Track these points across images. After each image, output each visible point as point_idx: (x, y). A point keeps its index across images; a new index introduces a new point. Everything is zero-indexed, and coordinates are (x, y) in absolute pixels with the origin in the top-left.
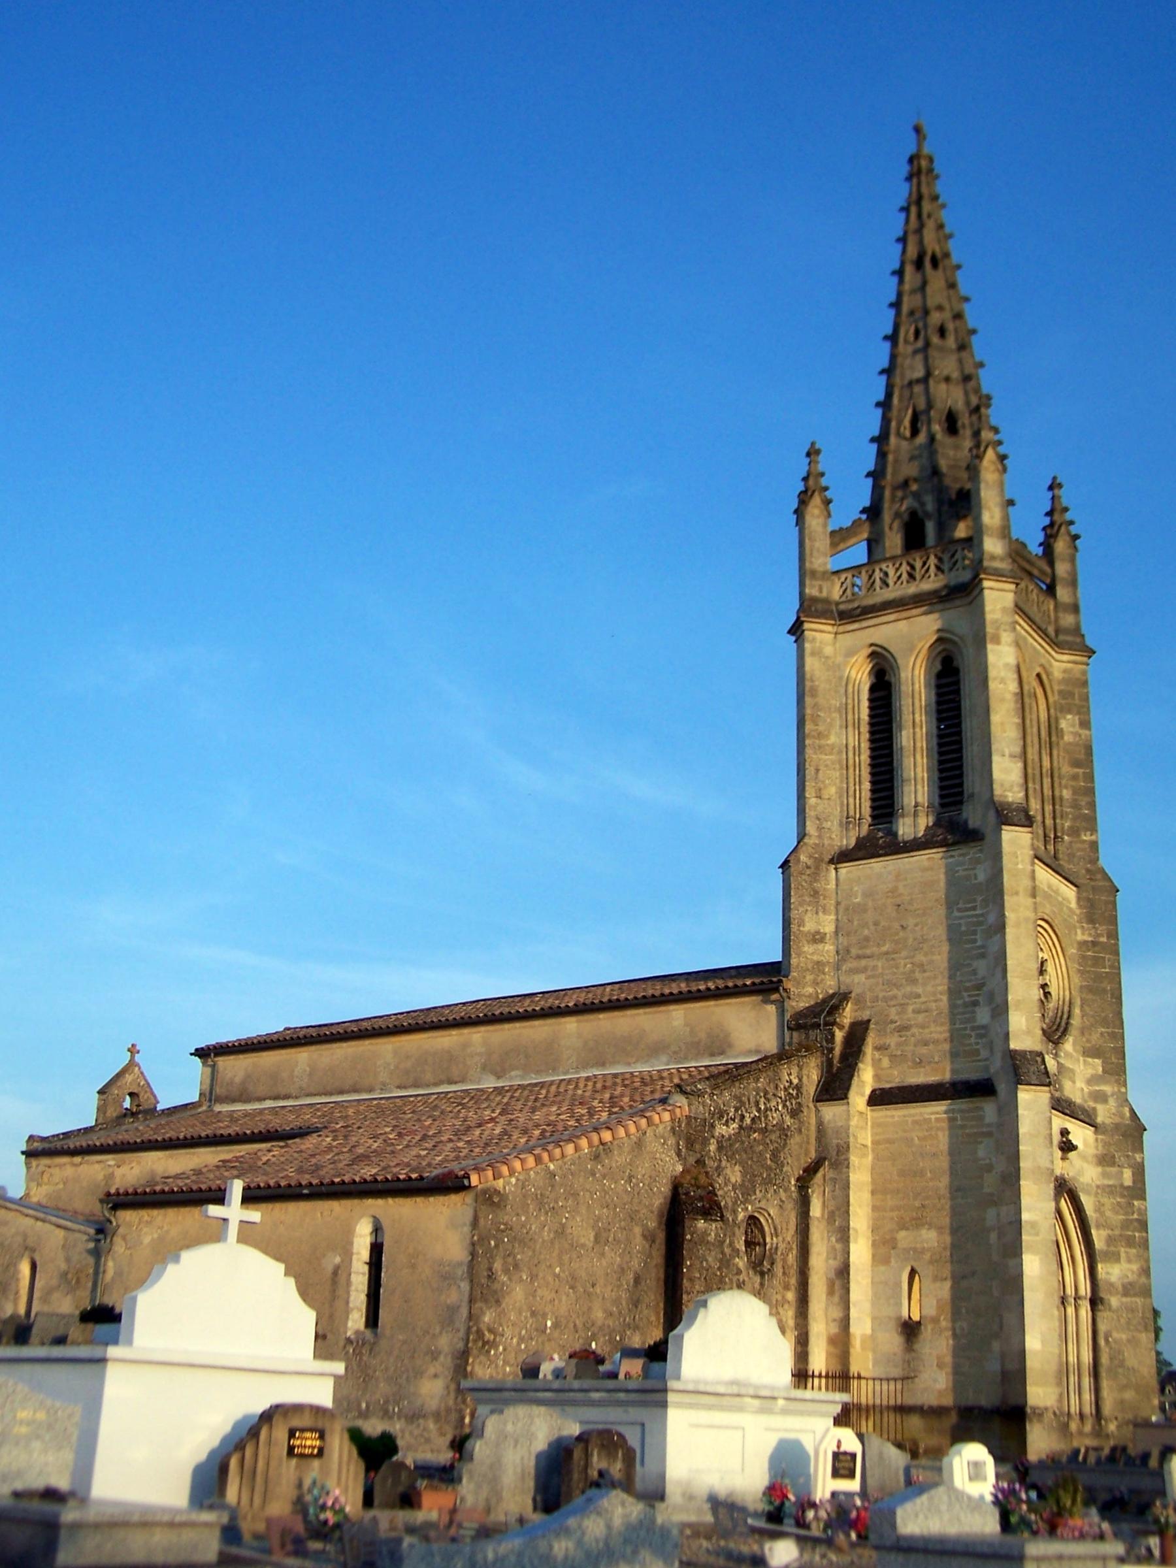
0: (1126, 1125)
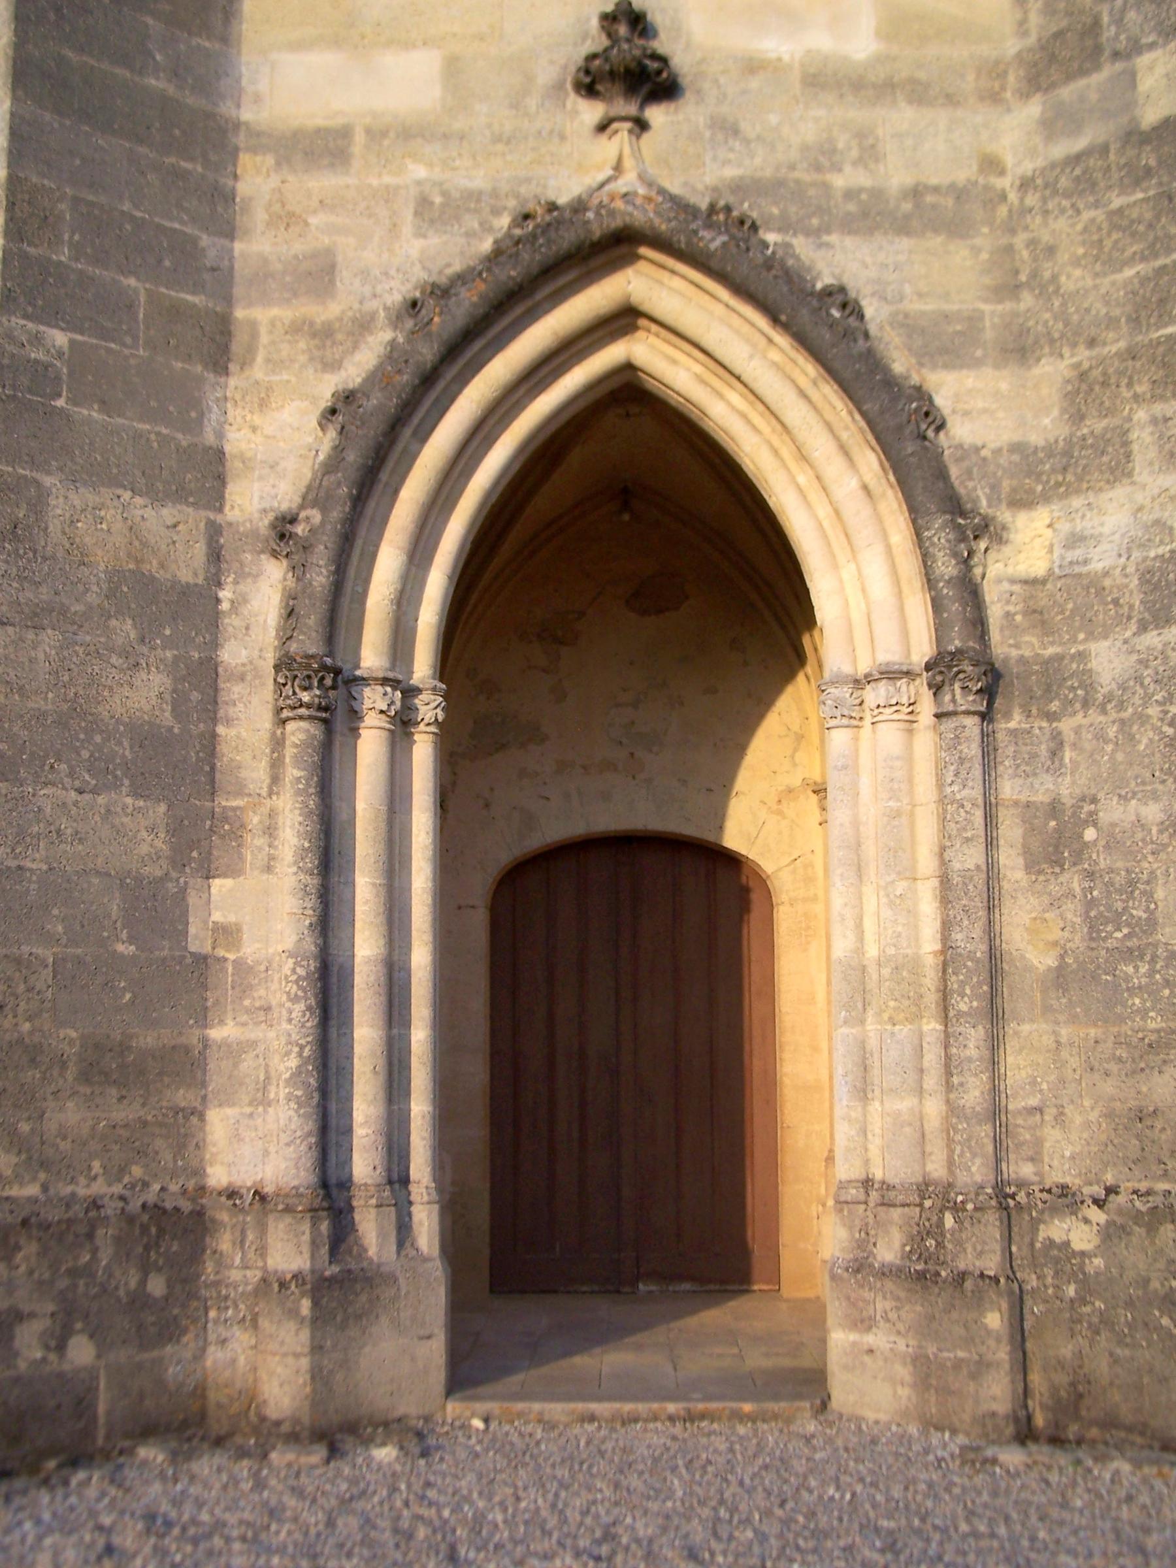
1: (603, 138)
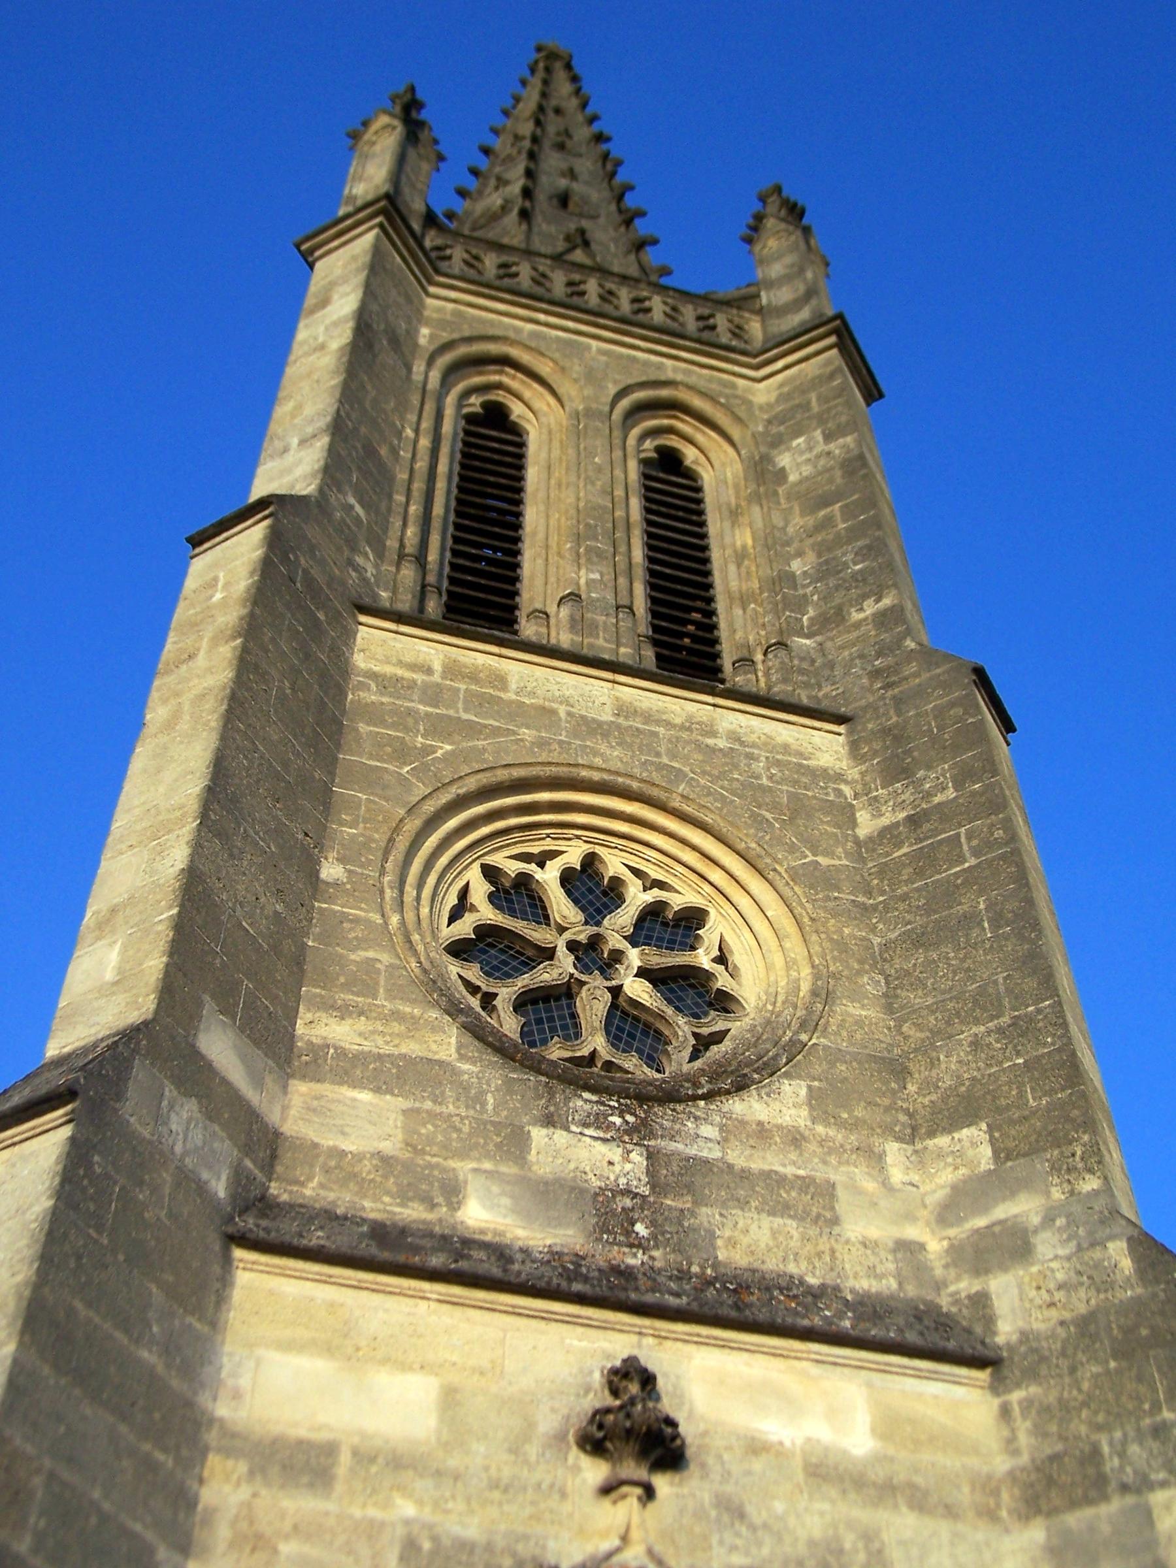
0: (1124, 1309)
1: (606, 1503)
